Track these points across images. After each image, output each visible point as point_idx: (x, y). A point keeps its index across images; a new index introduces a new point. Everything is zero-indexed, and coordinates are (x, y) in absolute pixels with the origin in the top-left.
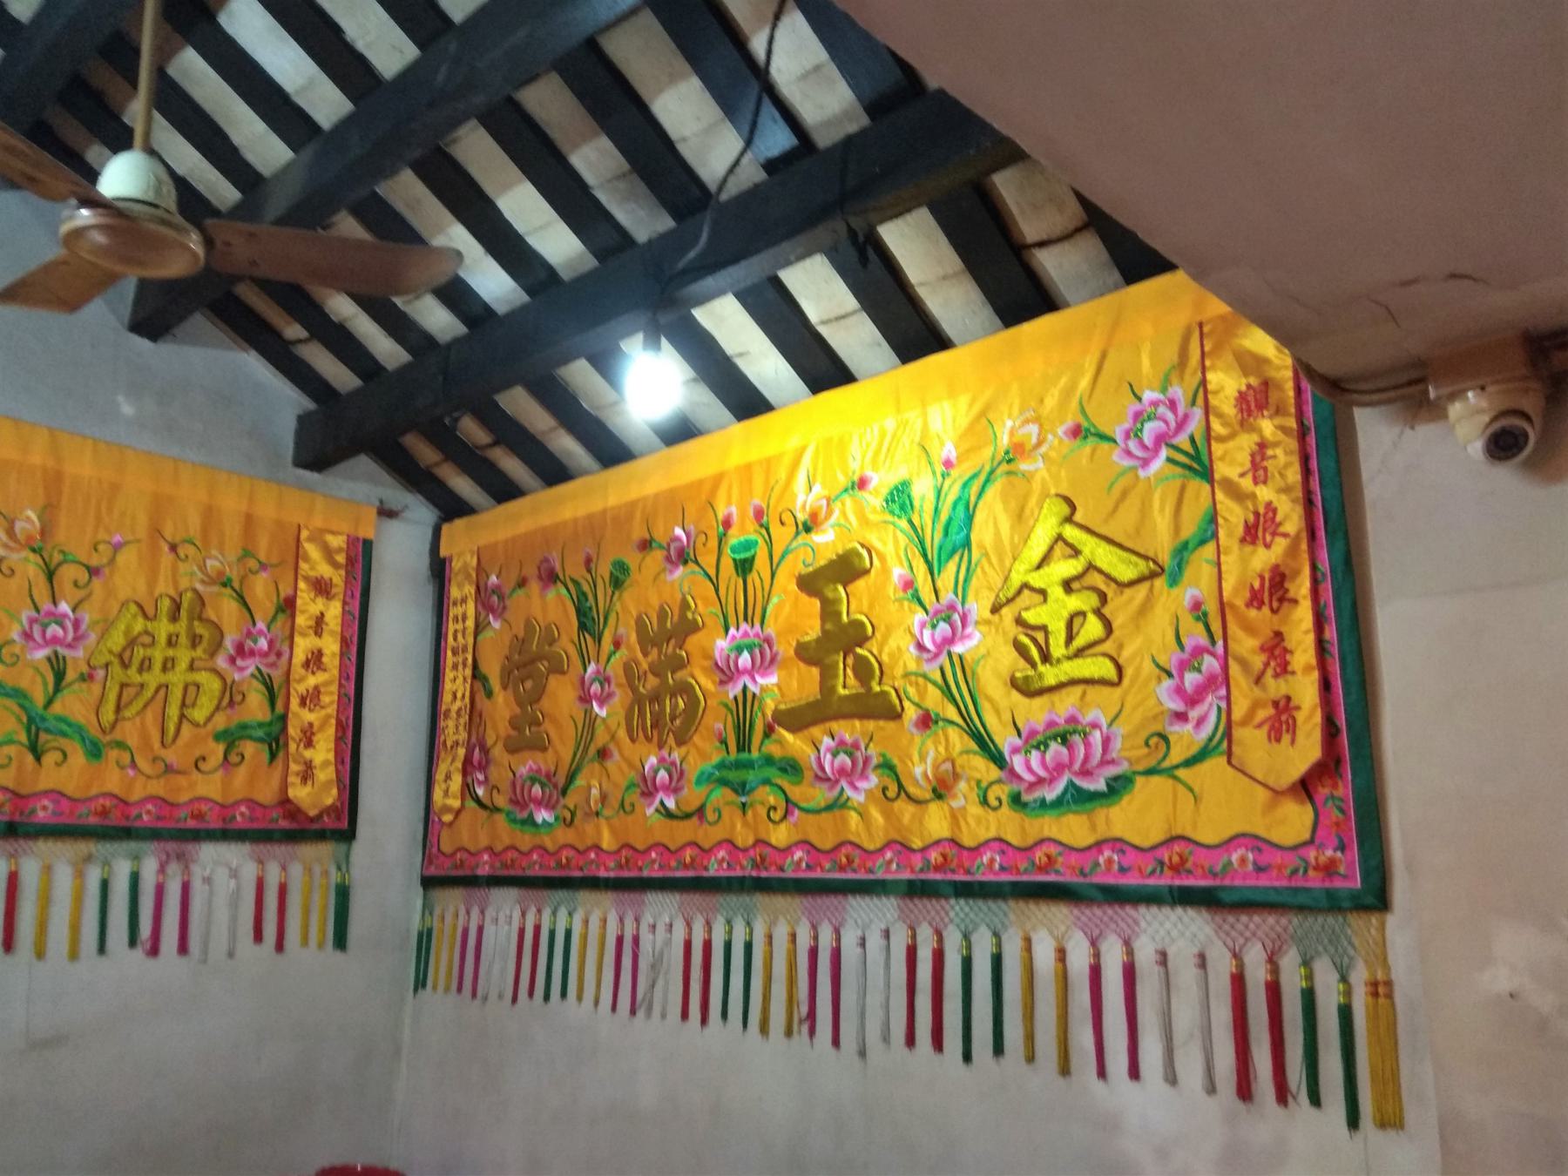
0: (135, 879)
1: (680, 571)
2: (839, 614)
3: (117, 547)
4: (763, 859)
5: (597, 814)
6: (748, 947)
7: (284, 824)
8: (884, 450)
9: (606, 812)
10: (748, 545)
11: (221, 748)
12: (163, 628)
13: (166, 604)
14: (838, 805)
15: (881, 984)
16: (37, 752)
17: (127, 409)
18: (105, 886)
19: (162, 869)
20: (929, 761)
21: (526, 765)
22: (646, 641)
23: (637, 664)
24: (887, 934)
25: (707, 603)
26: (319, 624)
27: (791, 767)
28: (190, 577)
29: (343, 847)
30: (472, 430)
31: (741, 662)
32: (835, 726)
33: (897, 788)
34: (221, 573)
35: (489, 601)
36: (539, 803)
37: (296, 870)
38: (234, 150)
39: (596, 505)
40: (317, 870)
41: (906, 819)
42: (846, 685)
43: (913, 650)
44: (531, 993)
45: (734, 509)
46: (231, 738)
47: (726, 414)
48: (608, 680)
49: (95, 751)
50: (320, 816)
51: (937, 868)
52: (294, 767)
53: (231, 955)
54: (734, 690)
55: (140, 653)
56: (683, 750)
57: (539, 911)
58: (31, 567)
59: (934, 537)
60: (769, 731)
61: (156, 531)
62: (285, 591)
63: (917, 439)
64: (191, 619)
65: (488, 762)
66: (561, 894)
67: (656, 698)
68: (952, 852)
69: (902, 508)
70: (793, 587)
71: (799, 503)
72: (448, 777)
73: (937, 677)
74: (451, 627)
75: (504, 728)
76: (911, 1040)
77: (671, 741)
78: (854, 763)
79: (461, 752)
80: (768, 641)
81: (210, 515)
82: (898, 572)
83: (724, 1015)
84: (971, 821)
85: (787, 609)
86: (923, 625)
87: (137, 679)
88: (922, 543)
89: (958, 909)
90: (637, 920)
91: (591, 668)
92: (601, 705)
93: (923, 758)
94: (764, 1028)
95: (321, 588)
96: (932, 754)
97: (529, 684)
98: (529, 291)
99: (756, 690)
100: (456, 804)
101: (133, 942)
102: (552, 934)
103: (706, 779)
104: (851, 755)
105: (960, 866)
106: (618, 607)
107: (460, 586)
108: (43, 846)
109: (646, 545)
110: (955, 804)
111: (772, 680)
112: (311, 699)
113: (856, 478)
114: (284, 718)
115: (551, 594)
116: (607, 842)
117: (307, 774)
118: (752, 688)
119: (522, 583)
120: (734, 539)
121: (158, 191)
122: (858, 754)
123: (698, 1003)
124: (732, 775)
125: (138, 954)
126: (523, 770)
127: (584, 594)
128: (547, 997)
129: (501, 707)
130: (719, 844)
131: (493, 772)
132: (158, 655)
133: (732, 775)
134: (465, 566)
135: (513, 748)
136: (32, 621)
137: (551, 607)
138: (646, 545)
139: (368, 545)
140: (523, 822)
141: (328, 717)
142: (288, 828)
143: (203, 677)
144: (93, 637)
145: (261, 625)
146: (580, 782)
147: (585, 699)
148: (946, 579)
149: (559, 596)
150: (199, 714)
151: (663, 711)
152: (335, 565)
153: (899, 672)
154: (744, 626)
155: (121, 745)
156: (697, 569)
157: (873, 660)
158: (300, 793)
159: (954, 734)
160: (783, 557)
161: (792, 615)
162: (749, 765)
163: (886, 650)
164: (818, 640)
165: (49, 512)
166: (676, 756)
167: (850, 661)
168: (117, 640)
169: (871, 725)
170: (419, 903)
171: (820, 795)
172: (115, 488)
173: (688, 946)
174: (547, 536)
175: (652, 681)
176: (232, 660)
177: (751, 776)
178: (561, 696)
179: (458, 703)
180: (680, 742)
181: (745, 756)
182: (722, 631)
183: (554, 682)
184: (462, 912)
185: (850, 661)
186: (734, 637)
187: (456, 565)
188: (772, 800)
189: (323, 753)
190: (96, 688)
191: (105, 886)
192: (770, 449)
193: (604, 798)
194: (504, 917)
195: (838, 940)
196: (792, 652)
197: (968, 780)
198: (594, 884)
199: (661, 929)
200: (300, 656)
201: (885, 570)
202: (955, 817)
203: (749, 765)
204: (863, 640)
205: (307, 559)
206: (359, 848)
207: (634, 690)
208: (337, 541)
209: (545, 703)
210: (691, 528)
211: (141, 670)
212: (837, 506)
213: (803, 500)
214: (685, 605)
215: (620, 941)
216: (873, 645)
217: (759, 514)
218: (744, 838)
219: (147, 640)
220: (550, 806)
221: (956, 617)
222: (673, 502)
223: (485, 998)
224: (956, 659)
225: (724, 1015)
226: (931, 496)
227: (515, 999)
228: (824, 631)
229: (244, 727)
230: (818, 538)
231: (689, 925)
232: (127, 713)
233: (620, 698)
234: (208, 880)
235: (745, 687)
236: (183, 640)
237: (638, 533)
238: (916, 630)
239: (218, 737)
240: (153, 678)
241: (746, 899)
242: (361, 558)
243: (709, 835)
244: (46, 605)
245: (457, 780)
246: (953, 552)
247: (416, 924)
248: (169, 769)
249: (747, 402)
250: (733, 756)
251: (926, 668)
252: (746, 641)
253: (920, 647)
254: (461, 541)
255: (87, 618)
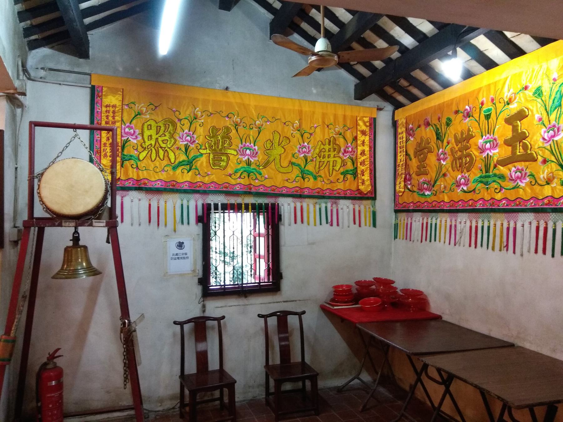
0: (326, 208)
1: (468, 119)
2: (518, 130)
3: (316, 127)
4: (493, 203)
5: (443, 192)
6: (489, 227)
7: (358, 195)
8: (534, 76)
9: (445, 192)
10: (489, 110)
11: (343, 176)
12: (327, 147)
13: (327, 141)
14: (516, 187)
15: (528, 236)
16: (304, 178)
17: (315, 91)
18: (320, 209)
19: (332, 206)
20: (545, 173)
21: (422, 179)
22: (457, 142)
23: (455, 148)
24: (530, 223)
25: (476, 128)
26: (363, 143)
27: (502, 177)
28: (332, 134)
29: (373, 201)
30: (403, 83)
31: (487, 146)
32: (516, 164)
33: (535, 182)
34: (339, 132)
35: (410, 132)
36: (426, 189)
37: (362, 207)
38: (337, 18)
39: (441, 101)
40: (367, 207)
41: (537, 191)
42: (520, 151)
43: (541, 140)
44: (426, 240)
45: (485, 99)
46: (344, 174)
47: (482, 68)
48: (445, 154)
49: (315, 178)
50: (367, 193)
51: (546, 204)
52: (360, 181)
53: (349, 227)
54: (485, 155)
55: (322, 154)
56: (469, 173)
57: (427, 219)
58: (297, 134)
59: (550, 103)
60: (495, 166)
61: (324, 122)
62: (355, 134)
63: (545, 72)
64: (333, 144)
65: (411, 179)
66: (434, 214)
67: (460, 158)
68: (551, 200)
69: (539, 95)
70: (503, 122)
71: (505, 96)
72: (400, 183)
73: (549, 148)
74: (399, 141)
75: (415, 169)
76: (536, 252)
77: (465, 171)
78: (522, 175)
79: (403, 176)
80: (495, 139)
81: (335, 116)
82: (537, 116)
83: (482, 246)
84: (558, 191)
85: (501, 130)
86: (545, 132)
87: (323, 160)
88: (545, 106)
89: (553, 216)
90: (456, 221)
91: (441, 150)
92: (444, 161)
93: (543, 173)
94: (493, 249)
95: (363, 133)
96: (546, 171)
97: (422, 156)
98: (418, 41)
99: (491, 154)
100: (403, 190)
101: (327, 223)
102: (431, 224)
103: (476, 181)
104: (521, 172)
105: (554, 204)
106: (448, 132)
107: (401, 128)
108: (307, 200)
109: (457, 112)
110: (553, 185)
111: (497, 151)
112: (363, 163)
113: (524, 86)
114: (356, 168)
115: (428, 129)
116: (446, 200)
117: (363, 183)
118: (490, 154)
119: (419, 126)
120: (485, 108)
121: (328, 47)
122: (523, 172)
123: (474, 242)
124: (484, 180)
125: (328, 225)
126: (421, 180)
127: (438, 129)
128: (430, 241)
129: (414, 163)
130: (480, 200)
131: (413, 181)
132: (327, 154)
133: (484, 180)
134: (402, 122)
135: (418, 175)
136: (300, 148)
137: (429, 133)
138: (457, 112)
139: (375, 119)
140: (422, 195)
141: (367, 167)
142: (358, 196)
143: (336, 159)
144: (312, 150)
145: (349, 144)
146: (438, 183)
147: (439, 160)
148: (553, 117)
149: (430, 129)
150: (337, 168)
151: (463, 162)
152: (367, 126)
153: (536, 147)
154: (488, 135)
155: (320, 176)
156: (473, 118)
157: (528, 143)
158: (362, 187)
159: (553, 165)
160: (500, 113)
161: (503, 131)
162: (489, 177)
163: (533, 140)
164: (511, 138)
165: (300, 120)
166: (467, 175)
167: (521, 144)
168: (317, 151)
169: (527, 163)
170: (394, 216)
171: (511, 185)
172: (314, 113)
173: (471, 227)
174: (426, 111)
175: (459, 153)
176: (343, 154)
177: (490, 180)
178: (432, 159)
179: (402, 162)
180: (468, 172)
181: (488, 174)
182: (481, 137)
183: (429, 155)
184: (406, 219)
185: (521, 144)
186: (484, 139)
187: (400, 122)
188: (496, 187)
189: (366, 177)
190: (314, 163)
191: (320, 209)
192: (496, 79)
193: (445, 187)
194: (417, 220)
195: (516, 225)
196: (503, 143)
197: (557, 178)
198: (443, 211)
199: (463, 223)
200: (359, 152)
201: (533, 115)
202: (553, 189)
203: (489, 177)
204: (525, 138)
205: (359, 125)
206: (378, 202)
207: (454, 156)
208: (367, 119)
209: (427, 161)
210: (471, 106)
211: (323, 158)
212: (518, 96)
213: (506, 95)
214: (469, 130)
215: (451, 226)
216: (528, 139)
217: (492, 100)
218: (487, 197)
219: (324, 150)
220: (430, 190)
221: (556, 129)
222: (465, 98)
223: (413, 241)
224: (555, 142)
225: (482, 246)
226: (549, 90)
227: (421, 242)
228: (513, 135)
229: (347, 171)
230: (511, 106)
231: (471, 222)
232: (322, 168)
233: (449, 159)
234: (342, 209)
235: (488, 154)
236: (332, 150)
237: (454, 108)
238: (542, 133)
239: (342, 174)
240: (326, 160)
241: (488, 214)
242: (373, 123)
243: (476, 197)
244: (302, 144)
245: (403, 184)
246: (556, 108)
247: (393, 222)
248: (331, 182)
249: (489, 64)
250: (484, 174)
251: (545, 145)
252: (488, 140)
253: (544, 139)
254: (401, 115)
255: (311, 146)
